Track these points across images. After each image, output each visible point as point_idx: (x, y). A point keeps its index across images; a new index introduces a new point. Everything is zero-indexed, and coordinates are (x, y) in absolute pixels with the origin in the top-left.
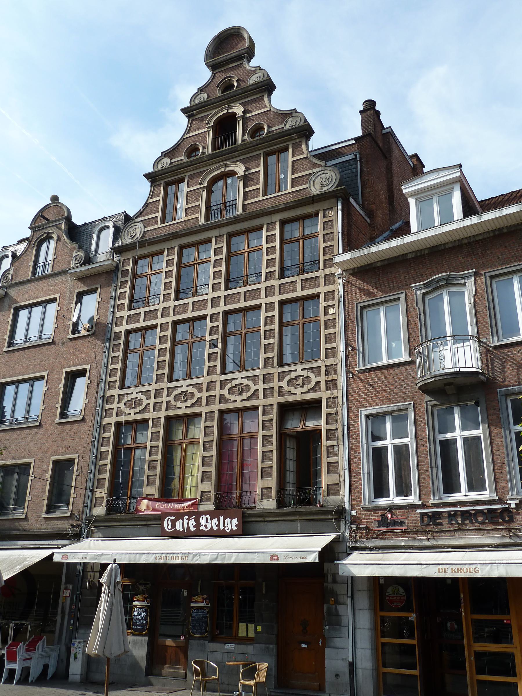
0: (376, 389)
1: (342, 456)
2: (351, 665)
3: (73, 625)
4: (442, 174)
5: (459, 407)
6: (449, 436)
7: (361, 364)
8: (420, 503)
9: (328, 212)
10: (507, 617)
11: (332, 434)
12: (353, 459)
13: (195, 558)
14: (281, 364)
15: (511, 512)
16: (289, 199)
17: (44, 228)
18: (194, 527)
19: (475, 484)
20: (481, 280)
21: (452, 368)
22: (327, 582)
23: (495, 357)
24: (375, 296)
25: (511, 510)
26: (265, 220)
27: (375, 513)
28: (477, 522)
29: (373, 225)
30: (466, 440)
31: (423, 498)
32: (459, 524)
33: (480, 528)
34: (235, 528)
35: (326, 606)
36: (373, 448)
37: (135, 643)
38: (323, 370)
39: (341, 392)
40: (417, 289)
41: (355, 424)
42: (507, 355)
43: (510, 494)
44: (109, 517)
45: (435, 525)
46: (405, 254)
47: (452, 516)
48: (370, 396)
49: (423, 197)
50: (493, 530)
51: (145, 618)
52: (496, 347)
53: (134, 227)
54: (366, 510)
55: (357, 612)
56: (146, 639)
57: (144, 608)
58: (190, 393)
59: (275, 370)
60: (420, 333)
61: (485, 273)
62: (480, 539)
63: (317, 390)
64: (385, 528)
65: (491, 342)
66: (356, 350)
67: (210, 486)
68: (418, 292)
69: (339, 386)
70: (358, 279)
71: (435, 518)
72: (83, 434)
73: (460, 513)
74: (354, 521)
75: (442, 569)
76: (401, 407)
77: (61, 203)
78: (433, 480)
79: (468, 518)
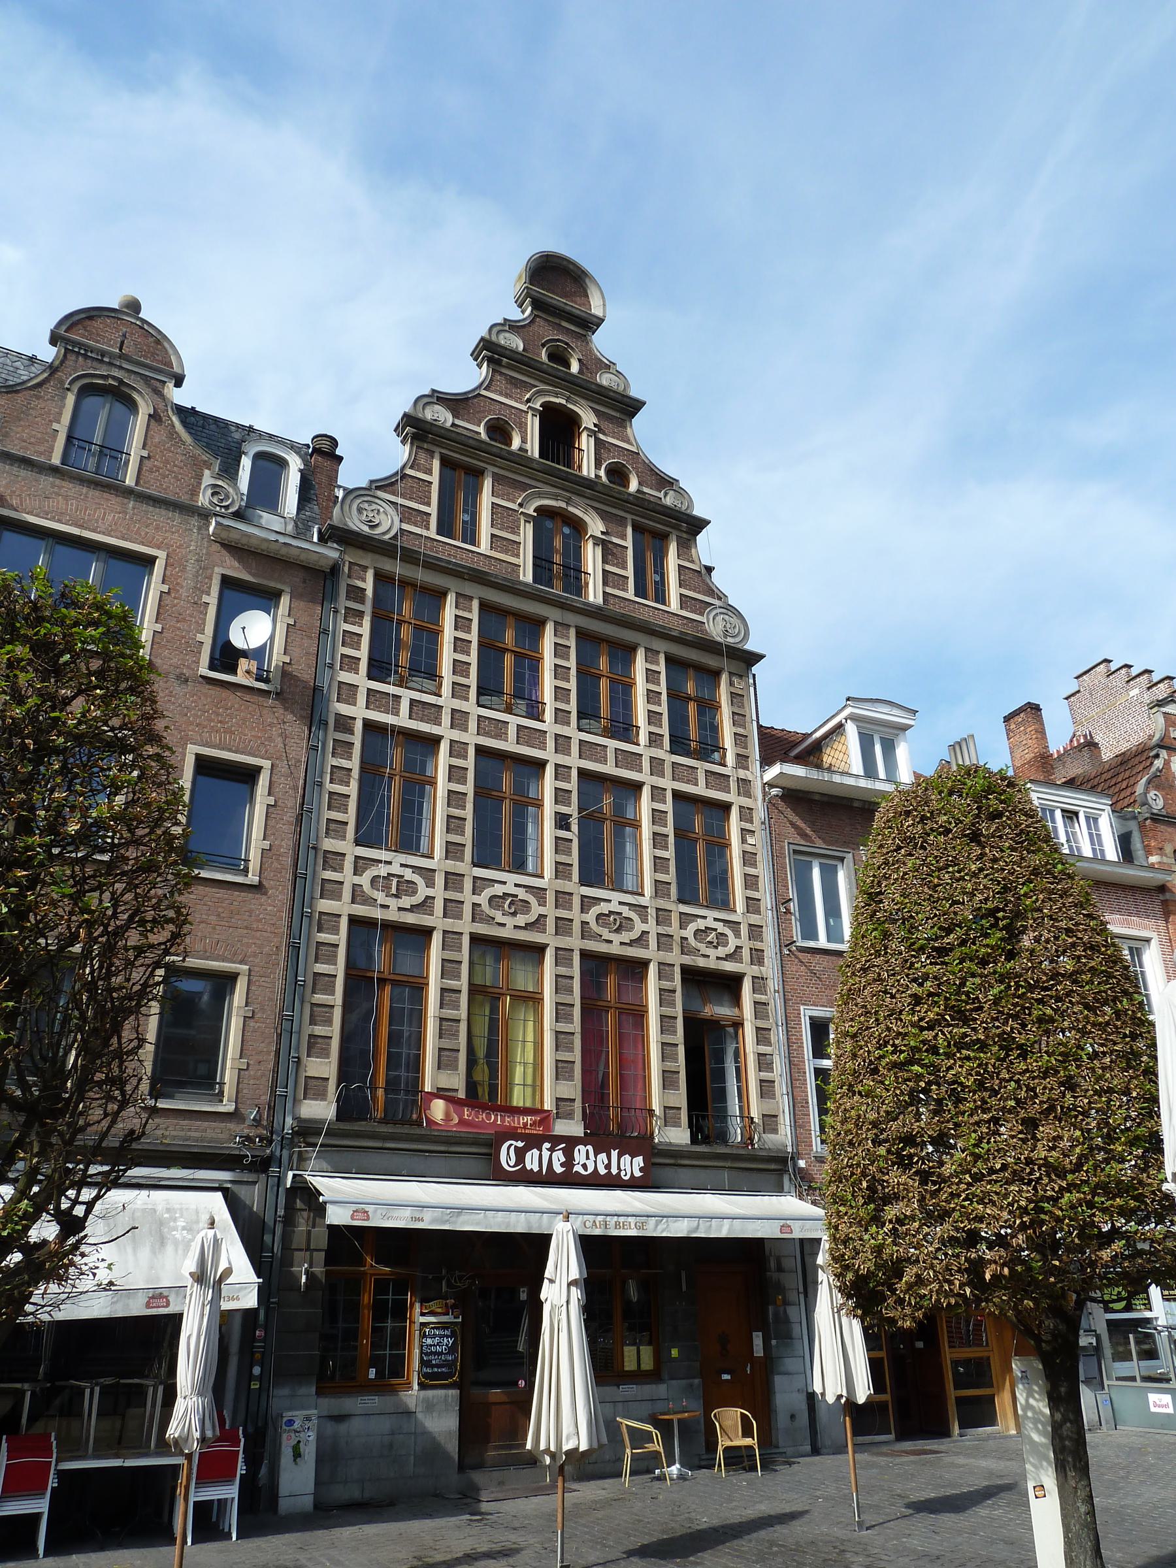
3: (260, 1378)
4: (896, 711)
13: (660, 1227)
17: (101, 361)
18: (562, 1165)
24: (813, 842)
34: (638, 1174)
35: (771, 1308)
37: (429, 1407)
44: (343, 1126)
51: (452, 1350)
53: (374, 507)
56: (454, 1393)
57: (447, 1328)
58: (522, 901)
67: (572, 1089)
72: (260, 921)
77: (144, 321)
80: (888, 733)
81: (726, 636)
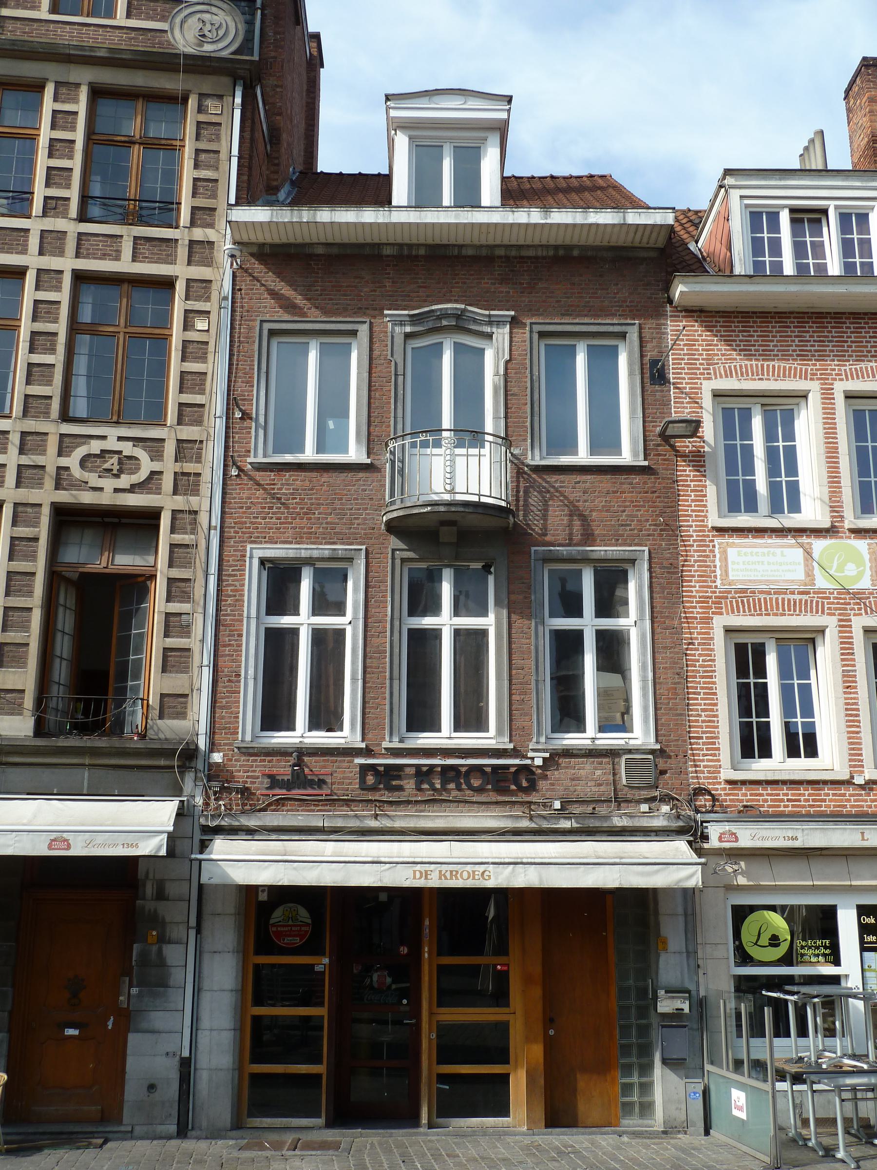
0: (288, 508)
1: (200, 637)
2: (186, 1066)
4: (473, 103)
5: (452, 570)
6: (428, 622)
7: (260, 451)
8: (363, 745)
9: (209, 102)
10: (503, 959)
11: (178, 589)
12: (225, 646)
14: (65, 417)
15: (533, 773)
16: (116, 40)
19: (470, 716)
20: (523, 334)
21: (490, 496)
22: (144, 898)
23: (532, 487)
24: (304, 315)
25: (534, 769)
26: (51, 71)
27: (264, 761)
28: (470, 787)
29: (276, 161)
30: (458, 633)
31: (370, 736)
32: (435, 790)
33: (474, 799)
36: (266, 629)
38: (170, 449)
39: (208, 503)
40: (394, 322)
41: (235, 575)
42: (554, 487)
43: (534, 740)
44: (40, 742)
45: (386, 786)
46: (379, 245)
47: (423, 775)
48: (274, 520)
49: (425, 137)
50: (497, 803)
52: (538, 469)
54: (244, 754)
55: (206, 957)
59: (54, 429)
60: (398, 413)
61: (531, 323)
62: (475, 820)
63: (151, 489)
64: (284, 791)
65: (530, 457)
66: (251, 419)
68: (397, 329)
69: (205, 489)
70: (270, 269)
71: (388, 777)
73: (439, 769)
74: (214, 773)
75: (421, 873)
76: (340, 554)
78: (391, 703)
79: (452, 779)
80: (467, 138)
81: (201, 44)
